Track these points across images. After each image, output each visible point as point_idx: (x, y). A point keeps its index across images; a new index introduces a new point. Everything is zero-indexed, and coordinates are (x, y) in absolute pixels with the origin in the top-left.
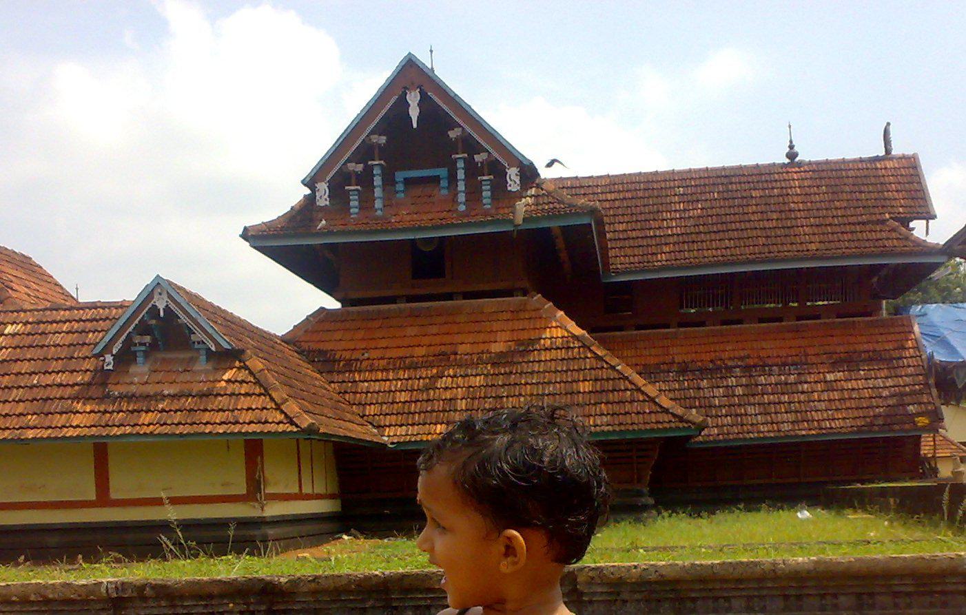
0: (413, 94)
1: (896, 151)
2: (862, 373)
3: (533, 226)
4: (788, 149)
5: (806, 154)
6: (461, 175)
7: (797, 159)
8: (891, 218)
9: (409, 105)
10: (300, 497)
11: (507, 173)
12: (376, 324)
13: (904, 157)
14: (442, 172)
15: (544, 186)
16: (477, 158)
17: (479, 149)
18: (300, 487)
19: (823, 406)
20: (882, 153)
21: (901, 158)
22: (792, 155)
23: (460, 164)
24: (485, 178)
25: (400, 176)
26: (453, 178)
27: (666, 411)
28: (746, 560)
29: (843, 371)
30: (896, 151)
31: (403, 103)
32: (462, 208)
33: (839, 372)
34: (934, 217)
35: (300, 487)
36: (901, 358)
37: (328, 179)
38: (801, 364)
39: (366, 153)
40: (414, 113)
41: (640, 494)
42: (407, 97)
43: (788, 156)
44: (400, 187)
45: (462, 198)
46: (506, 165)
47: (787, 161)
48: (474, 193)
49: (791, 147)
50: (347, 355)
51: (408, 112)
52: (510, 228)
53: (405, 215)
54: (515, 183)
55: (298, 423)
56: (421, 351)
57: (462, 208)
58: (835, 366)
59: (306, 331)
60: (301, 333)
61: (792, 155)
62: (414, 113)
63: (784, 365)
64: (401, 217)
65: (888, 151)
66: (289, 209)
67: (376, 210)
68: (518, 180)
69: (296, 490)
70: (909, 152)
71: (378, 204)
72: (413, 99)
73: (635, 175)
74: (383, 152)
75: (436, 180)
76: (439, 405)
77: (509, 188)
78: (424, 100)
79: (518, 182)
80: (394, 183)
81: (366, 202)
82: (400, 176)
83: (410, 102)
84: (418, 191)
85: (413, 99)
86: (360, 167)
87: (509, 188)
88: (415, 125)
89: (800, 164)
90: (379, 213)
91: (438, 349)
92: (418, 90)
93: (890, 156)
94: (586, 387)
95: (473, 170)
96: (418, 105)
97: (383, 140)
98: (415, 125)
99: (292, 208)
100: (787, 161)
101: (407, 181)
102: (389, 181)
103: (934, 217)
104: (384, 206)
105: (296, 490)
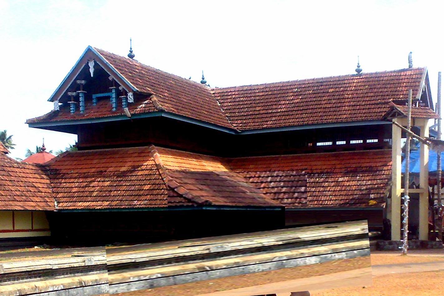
0: (91, 62)
1: (415, 66)
2: (358, 177)
3: (135, 117)
4: (357, 68)
7: (361, 73)
8: (393, 101)
9: (90, 68)
10: (32, 230)
11: (128, 95)
12: (83, 158)
13: (418, 69)
18: (14, 227)
20: (407, 67)
21: (416, 70)
22: (358, 71)
24: (122, 97)
25: (94, 96)
28: (76, 274)
29: (349, 177)
31: (87, 67)
32: (114, 109)
33: (346, 177)
35: (14, 227)
36: (382, 170)
37: (58, 99)
38: (329, 173)
39: (75, 87)
40: (92, 71)
42: (89, 64)
44: (94, 101)
46: (128, 91)
47: (356, 73)
50: (64, 172)
51: (89, 71)
53: (93, 114)
54: (131, 98)
56: (93, 170)
57: (114, 109)
58: (346, 174)
59: (56, 161)
60: (53, 162)
61: (358, 71)
62: (92, 71)
63: (321, 173)
64: (92, 114)
65: (410, 67)
66: (51, 111)
67: (81, 111)
68: (132, 97)
69: (12, 229)
70: (421, 66)
71: (81, 109)
72: (91, 65)
73: (320, 79)
74: (84, 87)
76: (87, 194)
77: (129, 101)
78: (96, 65)
79: (132, 99)
80: (92, 99)
81: (77, 107)
82: (94, 96)
83: (90, 66)
84: (101, 103)
85: (91, 65)
86: (74, 94)
87: (129, 101)
88: (92, 76)
89: (361, 75)
90: (82, 112)
91: (99, 170)
92: (93, 61)
93: (411, 68)
96: (94, 67)
97: (83, 82)
98: (92, 76)
99: (52, 111)
100: (356, 73)
101: (99, 99)
102: (88, 98)
104: (85, 109)
105: (12, 229)
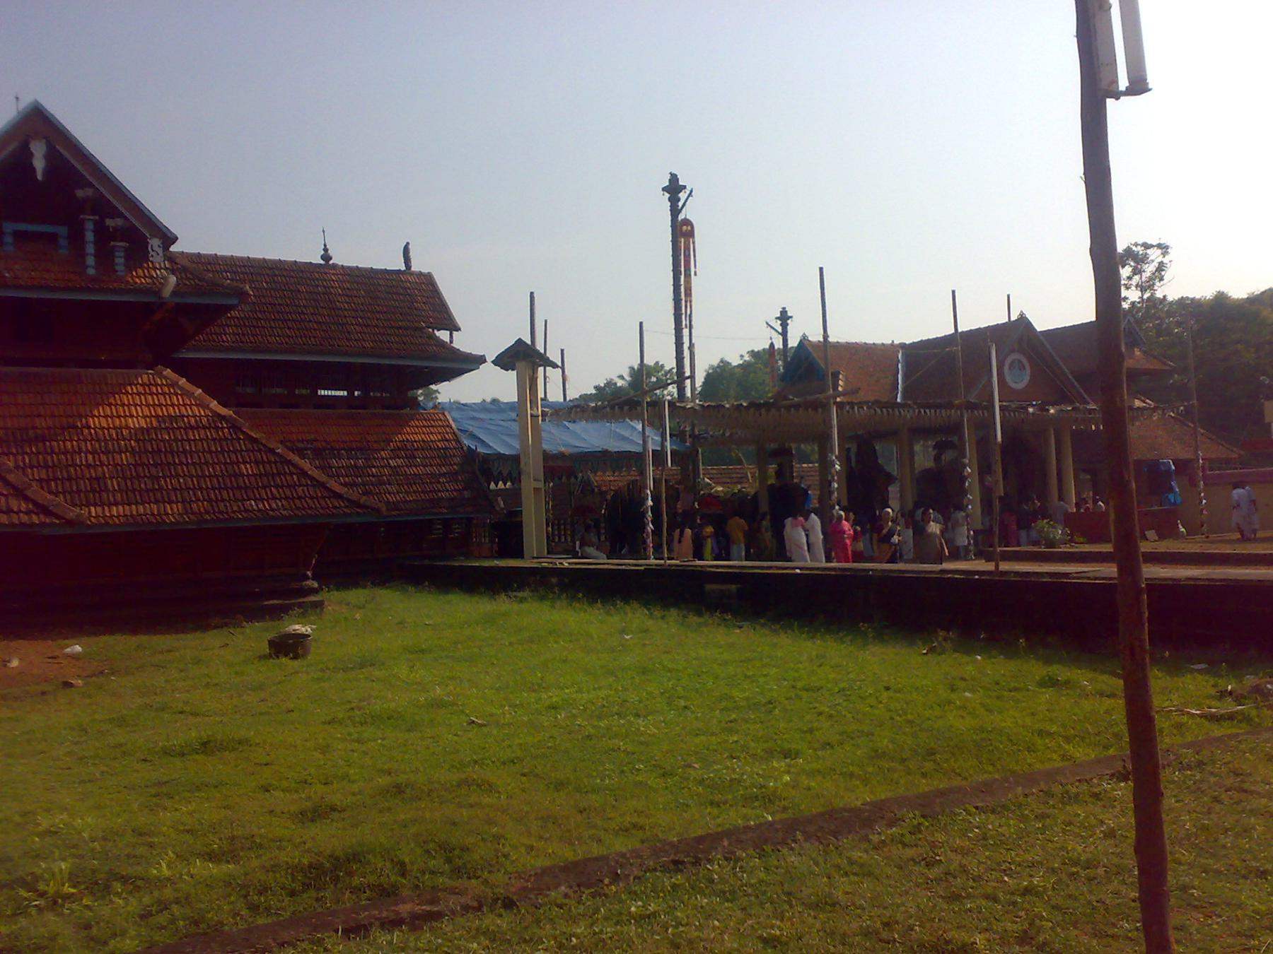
1: (415, 267)
5: (339, 259)
6: (90, 236)
7: (173, 248)
13: (421, 274)
14: (63, 231)
15: (178, 261)
16: (109, 222)
17: (115, 213)
19: (393, 489)
22: (327, 257)
23: (89, 226)
26: (76, 237)
27: (339, 496)
30: (415, 267)
34: (458, 329)
40: (39, 164)
41: (306, 578)
43: (322, 257)
45: (91, 261)
48: (104, 255)
49: (326, 250)
52: (152, 299)
55: (60, 513)
57: (91, 272)
61: (327, 257)
62: (39, 164)
75: (52, 238)
78: (52, 155)
85: (39, 153)
94: (247, 469)
95: (104, 238)
101: (18, 235)
103: (458, 329)
